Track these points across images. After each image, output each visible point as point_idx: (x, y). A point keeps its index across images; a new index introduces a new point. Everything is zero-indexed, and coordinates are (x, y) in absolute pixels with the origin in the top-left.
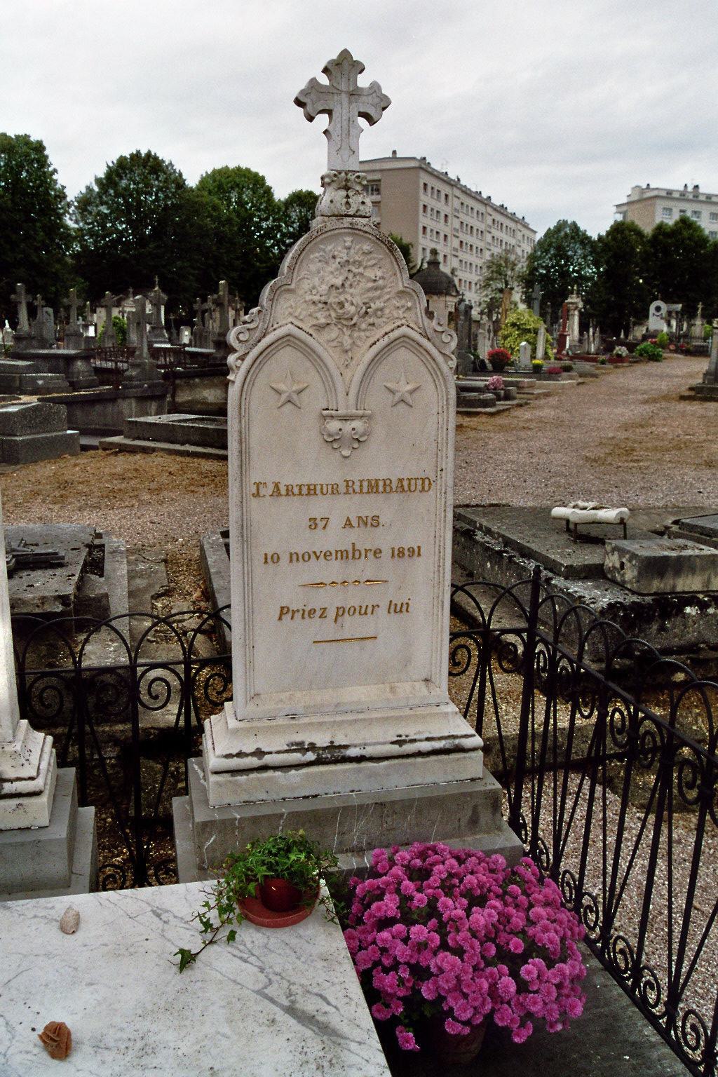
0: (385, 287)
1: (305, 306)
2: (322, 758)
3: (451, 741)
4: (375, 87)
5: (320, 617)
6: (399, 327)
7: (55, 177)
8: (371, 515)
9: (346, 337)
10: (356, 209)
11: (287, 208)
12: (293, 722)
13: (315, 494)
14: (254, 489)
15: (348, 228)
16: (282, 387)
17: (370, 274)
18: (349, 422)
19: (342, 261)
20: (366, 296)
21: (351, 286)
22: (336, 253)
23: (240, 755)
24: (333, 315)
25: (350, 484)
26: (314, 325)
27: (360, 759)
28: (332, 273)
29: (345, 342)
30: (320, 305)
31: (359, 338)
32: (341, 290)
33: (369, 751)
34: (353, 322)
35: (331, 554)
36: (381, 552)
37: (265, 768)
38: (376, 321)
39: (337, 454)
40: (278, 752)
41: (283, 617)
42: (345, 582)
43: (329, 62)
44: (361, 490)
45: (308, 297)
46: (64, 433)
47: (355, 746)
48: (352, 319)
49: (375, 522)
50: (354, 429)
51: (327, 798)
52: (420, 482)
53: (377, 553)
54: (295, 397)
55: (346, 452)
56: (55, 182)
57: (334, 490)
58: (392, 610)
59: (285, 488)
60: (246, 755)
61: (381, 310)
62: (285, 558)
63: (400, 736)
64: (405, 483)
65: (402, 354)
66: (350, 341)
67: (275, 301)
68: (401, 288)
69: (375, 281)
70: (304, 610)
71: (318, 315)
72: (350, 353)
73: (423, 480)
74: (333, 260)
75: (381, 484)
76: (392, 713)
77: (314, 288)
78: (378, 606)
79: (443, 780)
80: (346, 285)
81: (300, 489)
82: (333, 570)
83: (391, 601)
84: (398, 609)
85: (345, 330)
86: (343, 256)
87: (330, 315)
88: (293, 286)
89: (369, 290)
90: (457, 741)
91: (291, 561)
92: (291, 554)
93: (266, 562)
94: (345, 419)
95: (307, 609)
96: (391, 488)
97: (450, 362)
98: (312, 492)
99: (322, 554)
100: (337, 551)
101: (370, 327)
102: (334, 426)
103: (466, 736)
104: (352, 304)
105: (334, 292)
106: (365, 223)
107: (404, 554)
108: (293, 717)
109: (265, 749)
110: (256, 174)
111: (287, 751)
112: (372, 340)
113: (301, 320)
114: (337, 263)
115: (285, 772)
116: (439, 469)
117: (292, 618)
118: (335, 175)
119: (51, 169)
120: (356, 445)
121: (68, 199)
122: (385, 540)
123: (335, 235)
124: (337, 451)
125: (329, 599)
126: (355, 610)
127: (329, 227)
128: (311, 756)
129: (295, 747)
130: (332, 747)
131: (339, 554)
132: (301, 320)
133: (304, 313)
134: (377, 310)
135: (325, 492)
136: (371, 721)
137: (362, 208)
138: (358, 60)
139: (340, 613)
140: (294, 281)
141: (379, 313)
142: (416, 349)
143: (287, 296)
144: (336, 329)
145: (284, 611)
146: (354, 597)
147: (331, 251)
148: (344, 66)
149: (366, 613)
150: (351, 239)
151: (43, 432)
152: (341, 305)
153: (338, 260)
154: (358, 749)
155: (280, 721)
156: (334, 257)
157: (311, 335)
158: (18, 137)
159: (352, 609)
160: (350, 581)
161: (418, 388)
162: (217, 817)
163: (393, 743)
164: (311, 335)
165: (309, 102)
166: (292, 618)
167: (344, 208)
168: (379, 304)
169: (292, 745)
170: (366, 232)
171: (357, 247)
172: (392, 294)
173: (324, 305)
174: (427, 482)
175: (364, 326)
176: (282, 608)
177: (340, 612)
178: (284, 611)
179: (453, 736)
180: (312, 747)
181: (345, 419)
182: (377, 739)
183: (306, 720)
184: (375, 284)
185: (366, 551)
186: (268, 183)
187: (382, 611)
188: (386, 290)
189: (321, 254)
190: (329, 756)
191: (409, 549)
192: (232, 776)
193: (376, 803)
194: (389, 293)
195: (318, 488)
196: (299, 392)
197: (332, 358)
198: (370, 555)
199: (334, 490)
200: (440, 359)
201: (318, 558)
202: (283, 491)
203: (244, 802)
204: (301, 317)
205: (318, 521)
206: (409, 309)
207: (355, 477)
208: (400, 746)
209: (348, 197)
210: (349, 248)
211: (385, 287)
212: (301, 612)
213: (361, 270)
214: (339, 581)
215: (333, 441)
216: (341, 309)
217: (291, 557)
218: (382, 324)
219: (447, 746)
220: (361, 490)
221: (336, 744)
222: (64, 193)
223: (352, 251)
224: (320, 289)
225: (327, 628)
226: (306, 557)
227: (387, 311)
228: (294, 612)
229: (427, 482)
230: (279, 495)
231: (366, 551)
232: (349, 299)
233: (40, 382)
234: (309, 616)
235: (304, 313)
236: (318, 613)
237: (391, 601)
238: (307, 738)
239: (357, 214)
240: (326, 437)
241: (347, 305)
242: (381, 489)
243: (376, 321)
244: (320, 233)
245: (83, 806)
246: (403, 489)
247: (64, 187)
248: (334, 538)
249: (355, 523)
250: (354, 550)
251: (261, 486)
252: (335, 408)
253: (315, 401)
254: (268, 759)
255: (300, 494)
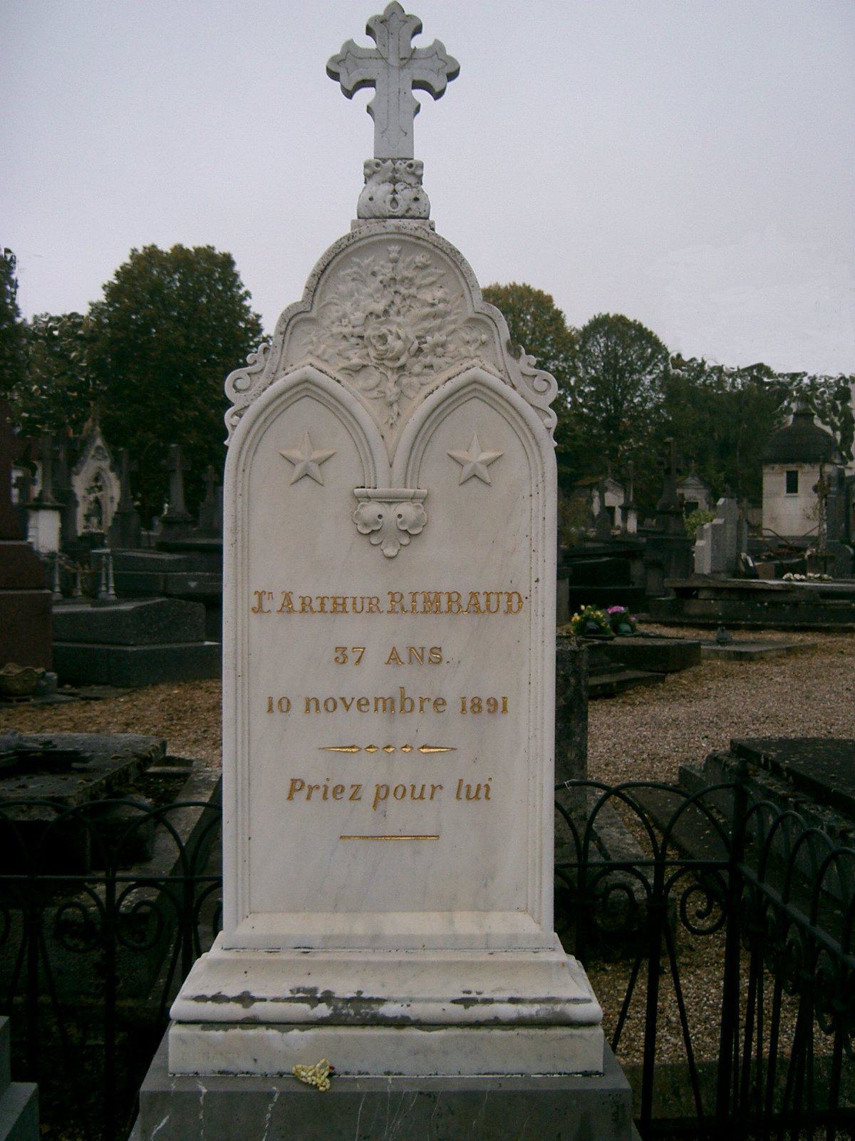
0: (447, 313)
1: (331, 341)
2: (341, 1015)
3: (549, 1007)
4: (437, 50)
5: (351, 798)
6: (468, 369)
7: (247, 303)
8: (429, 646)
9: (391, 384)
10: (406, 208)
11: (585, 342)
12: (305, 957)
13: (345, 611)
14: (254, 602)
15: (395, 233)
16: (296, 454)
17: (427, 296)
18: (393, 506)
19: (386, 278)
20: (420, 327)
21: (398, 313)
22: (376, 268)
23: (218, 998)
24: (373, 353)
25: (397, 597)
26: (344, 369)
27: (401, 1023)
28: (371, 296)
29: (388, 393)
30: (353, 340)
31: (410, 386)
32: (383, 318)
33: (416, 1011)
34: (398, 364)
35: (368, 703)
36: (444, 703)
37: (252, 1022)
38: (436, 361)
39: (376, 550)
40: (276, 1000)
41: (296, 795)
42: (388, 747)
43: (371, 20)
44: (414, 608)
45: (335, 330)
46: (199, 644)
47: (396, 1002)
48: (399, 359)
49: (435, 656)
50: (400, 516)
51: (347, 1080)
52: (504, 598)
53: (439, 703)
54: (315, 469)
55: (390, 551)
56: (247, 309)
57: (372, 606)
58: (463, 794)
59: (301, 600)
60: (228, 1000)
61: (443, 345)
62: (298, 706)
63: (469, 992)
64: (482, 600)
65: (475, 409)
66: (396, 390)
67: (288, 334)
68: (471, 314)
69: (433, 305)
70: (326, 787)
71: (351, 354)
72: (395, 407)
73: (510, 595)
74: (373, 279)
75: (444, 599)
76: (458, 957)
77: (345, 316)
78: (441, 787)
79: (537, 1070)
80: (392, 312)
81: (322, 604)
82: (371, 727)
83: (461, 781)
84: (473, 794)
85: (389, 373)
86: (387, 272)
87: (368, 355)
88: (313, 314)
89: (426, 317)
90: (558, 1008)
91: (308, 709)
92: (308, 701)
93: (270, 710)
94: (390, 500)
95: (331, 786)
96: (460, 606)
97: (547, 420)
98: (340, 608)
99: (355, 702)
100: (377, 700)
101: (426, 371)
102: (372, 509)
103: (576, 1001)
104: (399, 338)
105: (373, 320)
106: (416, 226)
107: (480, 707)
108: (307, 950)
109: (255, 994)
110: (540, 293)
111: (289, 1000)
112: (428, 389)
113: (326, 361)
114: (378, 282)
115: (283, 1032)
116: (534, 579)
117: (308, 798)
118: (378, 165)
119: (241, 292)
120: (405, 541)
121: (264, 334)
122: (453, 686)
123: (373, 243)
124: (377, 548)
125: (367, 771)
126: (405, 790)
127: (365, 232)
128: (323, 1010)
129: (301, 995)
130: (358, 1000)
131: (380, 703)
132: (326, 361)
133: (330, 351)
134: (437, 345)
135: (359, 609)
136: (422, 968)
137: (414, 206)
138: (384, 7)
139: (382, 794)
140: (315, 308)
141: (440, 350)
142: (495, 401)
143: (305, 327)
144: (377, 373)
145: (296, 786)
146: (403, 772)
147: (369, 265)
148: (393, 26)
149: (421, 797)
150: (397, 248)
151: (169, 642)
152: (383, 338)
153: (380, 278)
154: (398, 1005)
155: (285, 956)
156: (374, 274)
157: (339, 381)
158: (198, 250)
159: (400, 790)
160: (398, 746)
161: (500, 457)
162: (173, 1087)
163: (454, 1002)
164: (339, 381)
165: (347, 71)
166: (308, 798)
167: (388, 206)
168: (439, 337)
169: (298, 991)
170: (419, 238)
171: (408, 259)
172: (460, 322)
173: (359, 341)
174: (515, 598)
175: (417, 369)
176: (294, 781)
177: (383, 793)
178: (296, 786)
179: (553, 998)
180: (328, 998)
181: (390, 500)
182: (431, 994)
183: (322, 957)
184: (433, 310)
185: (422, 700)
186: (558, 305)
187: (447, 795)
188: (449, 318)
189: (355, 269)
190: (352, 1012)
191: (488, 700)
192: (203, 1029)
193: (421, 1093)
194: (454, 322)
195: (349, 602)
196: (321, 463)
197: (367, 412)
198: (428, 706)
199: (372, 606)
200: (530, 413)
201: (348, 707)
202: (297, 605)
203: (220, 1072)
204: (326, 357)
205: (348, 652)
206: (483, 344)
207: (405, 587)
208: (466, 1007)
209: (395, 192)
210: (395, 261)
211: (447, 313)
212: (322, 789)
213: (413, 291)
214: (381, 744)
215: (372, 532)
216: (384, 344)
217: (308, 704)
218: (444, 367)
219: (542, 1014)
220: (414, 608)
221: (364, 995)
222: (259, 325)
223: (401, 265)
224: (352, 317)
225: (362, 817)
226: (331, 705)
227: (451, 347)
228: (311, 788)
229: (515, 598)
230: (291, 611)
231: (422, 700)
232: (394, 331)
233: (193, 584)
234: (335, 796)
235: (330, 351)
236: (348, 792)
237: (461, 781)
238: (322, 984)
239: (407, 215)
240: (360, 528)
241: (390, 338)
242: (444, 607)
243: (436, 361)
244: (352, 241)
245: (22, 1081)
246: (479, 608)
247: (258, 317)
248: (370, 679)
249: (404, 656)
250: (403, 699)
251: (265, 597)
252: (373, 485)
253: (343, 476)
254: (257, 1009)
255: (322, 611)
